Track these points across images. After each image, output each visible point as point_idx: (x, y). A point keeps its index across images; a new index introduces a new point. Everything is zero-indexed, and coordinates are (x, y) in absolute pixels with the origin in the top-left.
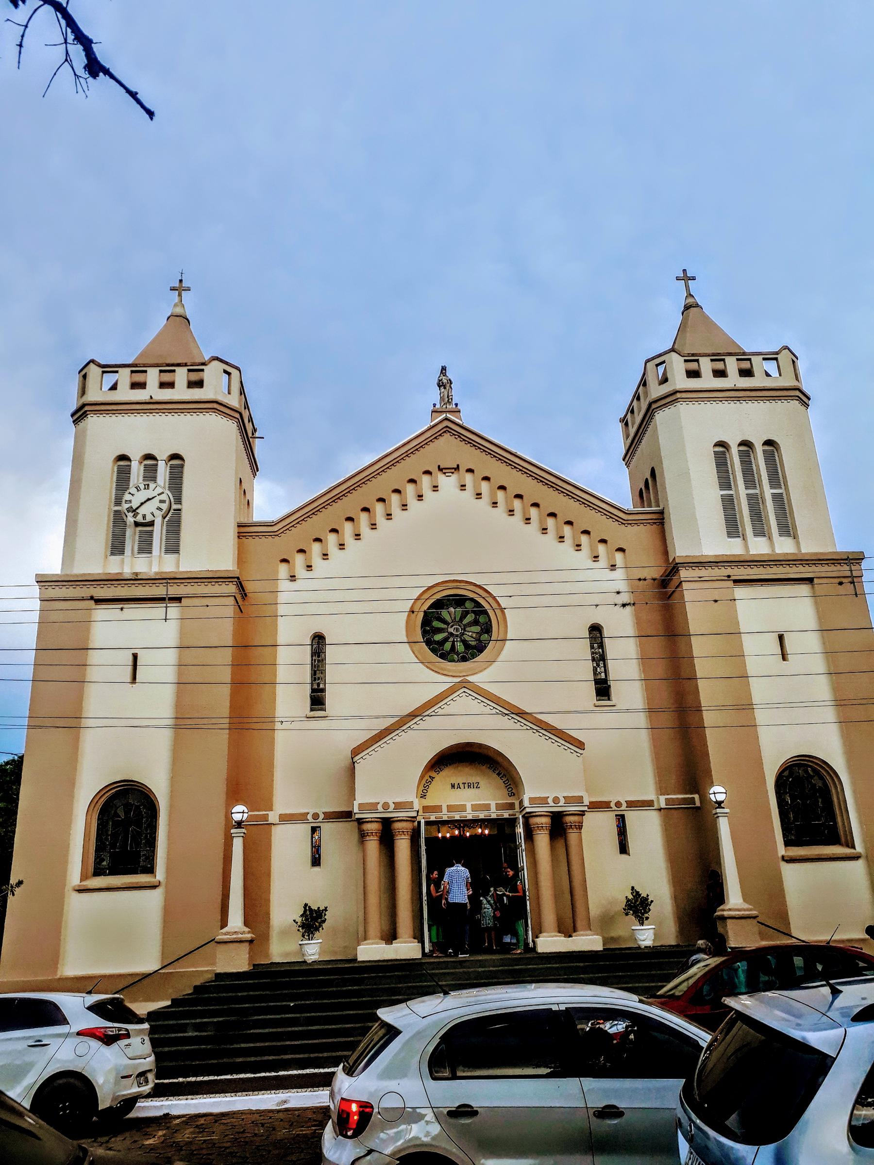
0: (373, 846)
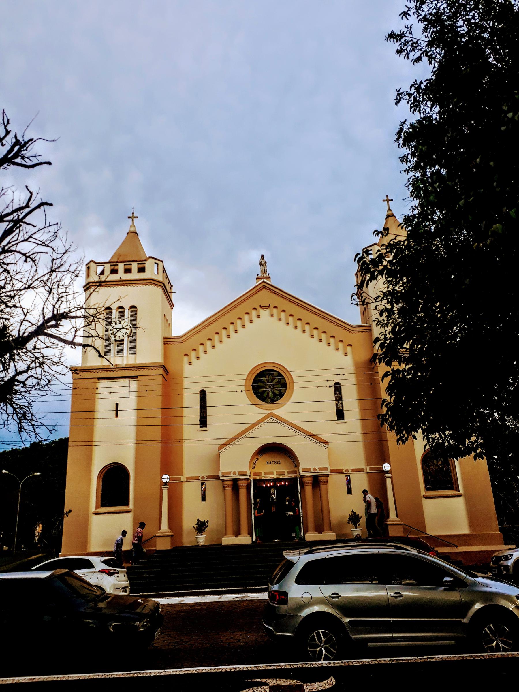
0: (229, 492)
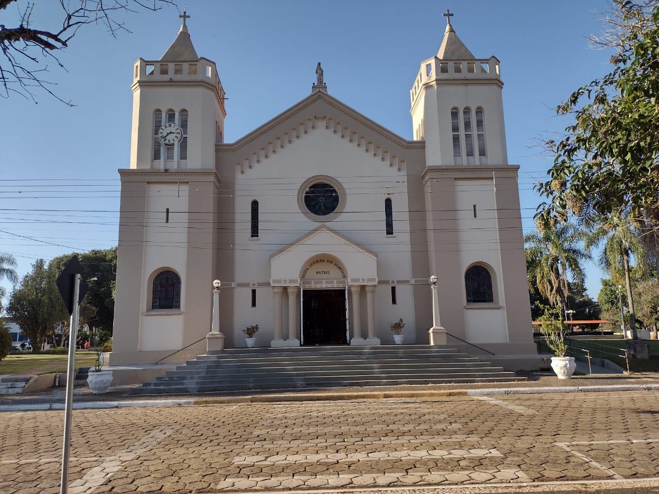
0: (278, 298)
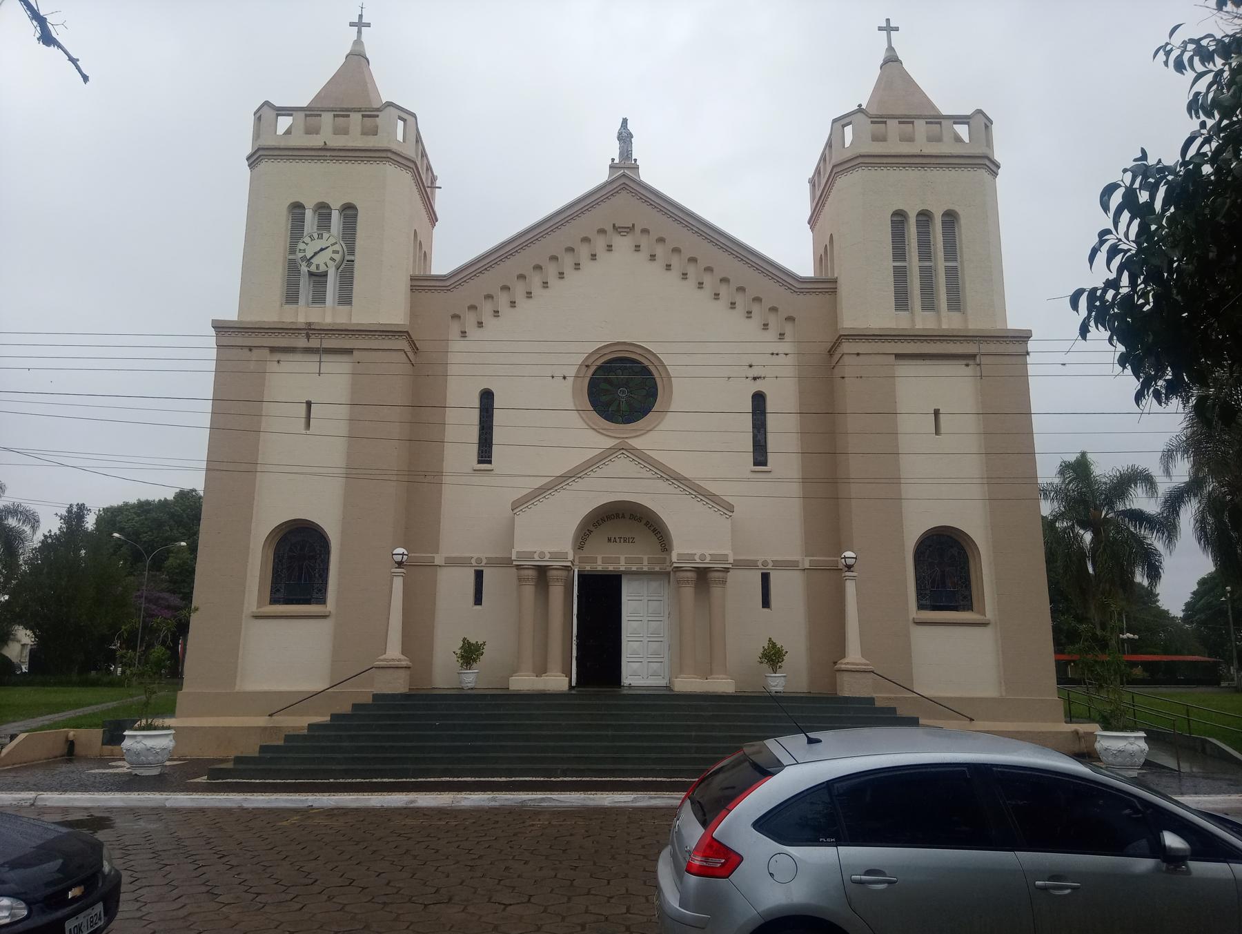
0: (529, 590)
